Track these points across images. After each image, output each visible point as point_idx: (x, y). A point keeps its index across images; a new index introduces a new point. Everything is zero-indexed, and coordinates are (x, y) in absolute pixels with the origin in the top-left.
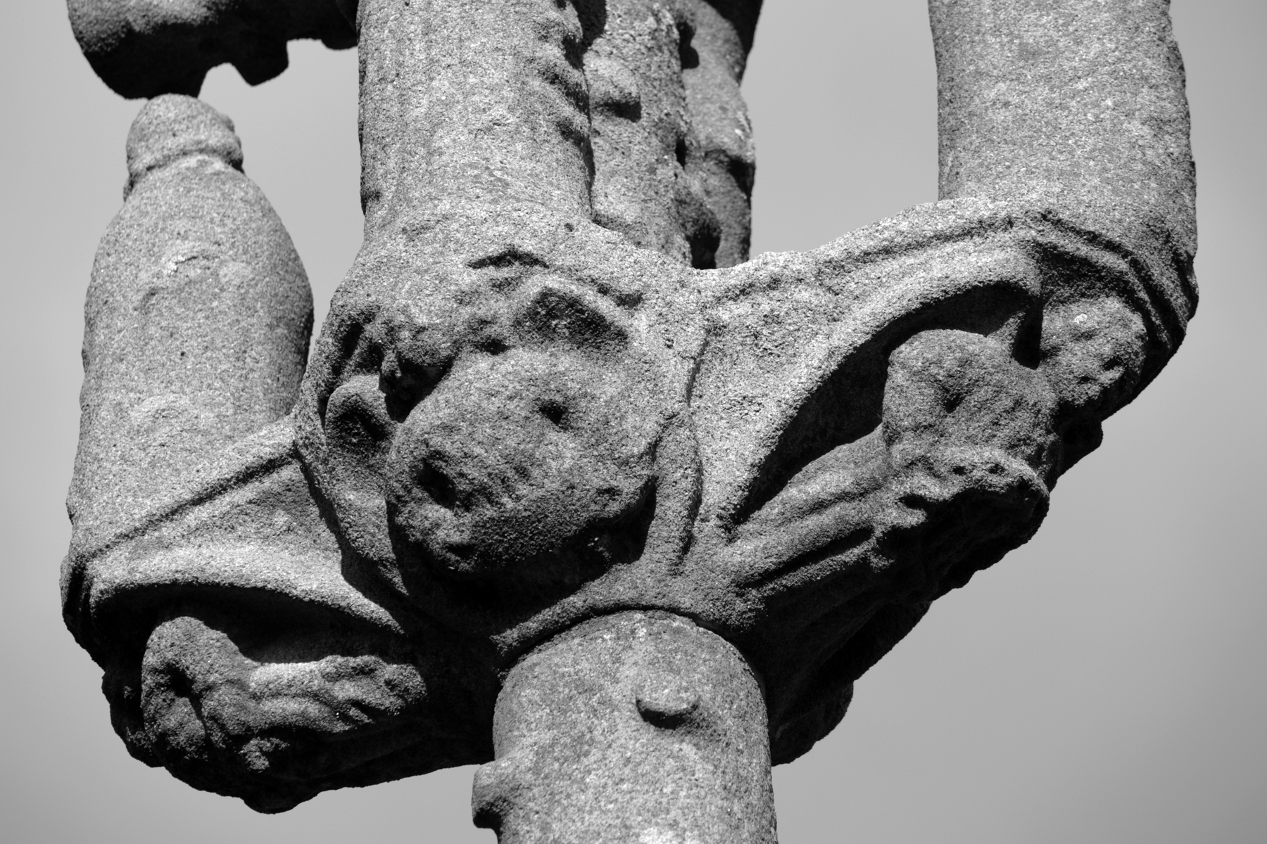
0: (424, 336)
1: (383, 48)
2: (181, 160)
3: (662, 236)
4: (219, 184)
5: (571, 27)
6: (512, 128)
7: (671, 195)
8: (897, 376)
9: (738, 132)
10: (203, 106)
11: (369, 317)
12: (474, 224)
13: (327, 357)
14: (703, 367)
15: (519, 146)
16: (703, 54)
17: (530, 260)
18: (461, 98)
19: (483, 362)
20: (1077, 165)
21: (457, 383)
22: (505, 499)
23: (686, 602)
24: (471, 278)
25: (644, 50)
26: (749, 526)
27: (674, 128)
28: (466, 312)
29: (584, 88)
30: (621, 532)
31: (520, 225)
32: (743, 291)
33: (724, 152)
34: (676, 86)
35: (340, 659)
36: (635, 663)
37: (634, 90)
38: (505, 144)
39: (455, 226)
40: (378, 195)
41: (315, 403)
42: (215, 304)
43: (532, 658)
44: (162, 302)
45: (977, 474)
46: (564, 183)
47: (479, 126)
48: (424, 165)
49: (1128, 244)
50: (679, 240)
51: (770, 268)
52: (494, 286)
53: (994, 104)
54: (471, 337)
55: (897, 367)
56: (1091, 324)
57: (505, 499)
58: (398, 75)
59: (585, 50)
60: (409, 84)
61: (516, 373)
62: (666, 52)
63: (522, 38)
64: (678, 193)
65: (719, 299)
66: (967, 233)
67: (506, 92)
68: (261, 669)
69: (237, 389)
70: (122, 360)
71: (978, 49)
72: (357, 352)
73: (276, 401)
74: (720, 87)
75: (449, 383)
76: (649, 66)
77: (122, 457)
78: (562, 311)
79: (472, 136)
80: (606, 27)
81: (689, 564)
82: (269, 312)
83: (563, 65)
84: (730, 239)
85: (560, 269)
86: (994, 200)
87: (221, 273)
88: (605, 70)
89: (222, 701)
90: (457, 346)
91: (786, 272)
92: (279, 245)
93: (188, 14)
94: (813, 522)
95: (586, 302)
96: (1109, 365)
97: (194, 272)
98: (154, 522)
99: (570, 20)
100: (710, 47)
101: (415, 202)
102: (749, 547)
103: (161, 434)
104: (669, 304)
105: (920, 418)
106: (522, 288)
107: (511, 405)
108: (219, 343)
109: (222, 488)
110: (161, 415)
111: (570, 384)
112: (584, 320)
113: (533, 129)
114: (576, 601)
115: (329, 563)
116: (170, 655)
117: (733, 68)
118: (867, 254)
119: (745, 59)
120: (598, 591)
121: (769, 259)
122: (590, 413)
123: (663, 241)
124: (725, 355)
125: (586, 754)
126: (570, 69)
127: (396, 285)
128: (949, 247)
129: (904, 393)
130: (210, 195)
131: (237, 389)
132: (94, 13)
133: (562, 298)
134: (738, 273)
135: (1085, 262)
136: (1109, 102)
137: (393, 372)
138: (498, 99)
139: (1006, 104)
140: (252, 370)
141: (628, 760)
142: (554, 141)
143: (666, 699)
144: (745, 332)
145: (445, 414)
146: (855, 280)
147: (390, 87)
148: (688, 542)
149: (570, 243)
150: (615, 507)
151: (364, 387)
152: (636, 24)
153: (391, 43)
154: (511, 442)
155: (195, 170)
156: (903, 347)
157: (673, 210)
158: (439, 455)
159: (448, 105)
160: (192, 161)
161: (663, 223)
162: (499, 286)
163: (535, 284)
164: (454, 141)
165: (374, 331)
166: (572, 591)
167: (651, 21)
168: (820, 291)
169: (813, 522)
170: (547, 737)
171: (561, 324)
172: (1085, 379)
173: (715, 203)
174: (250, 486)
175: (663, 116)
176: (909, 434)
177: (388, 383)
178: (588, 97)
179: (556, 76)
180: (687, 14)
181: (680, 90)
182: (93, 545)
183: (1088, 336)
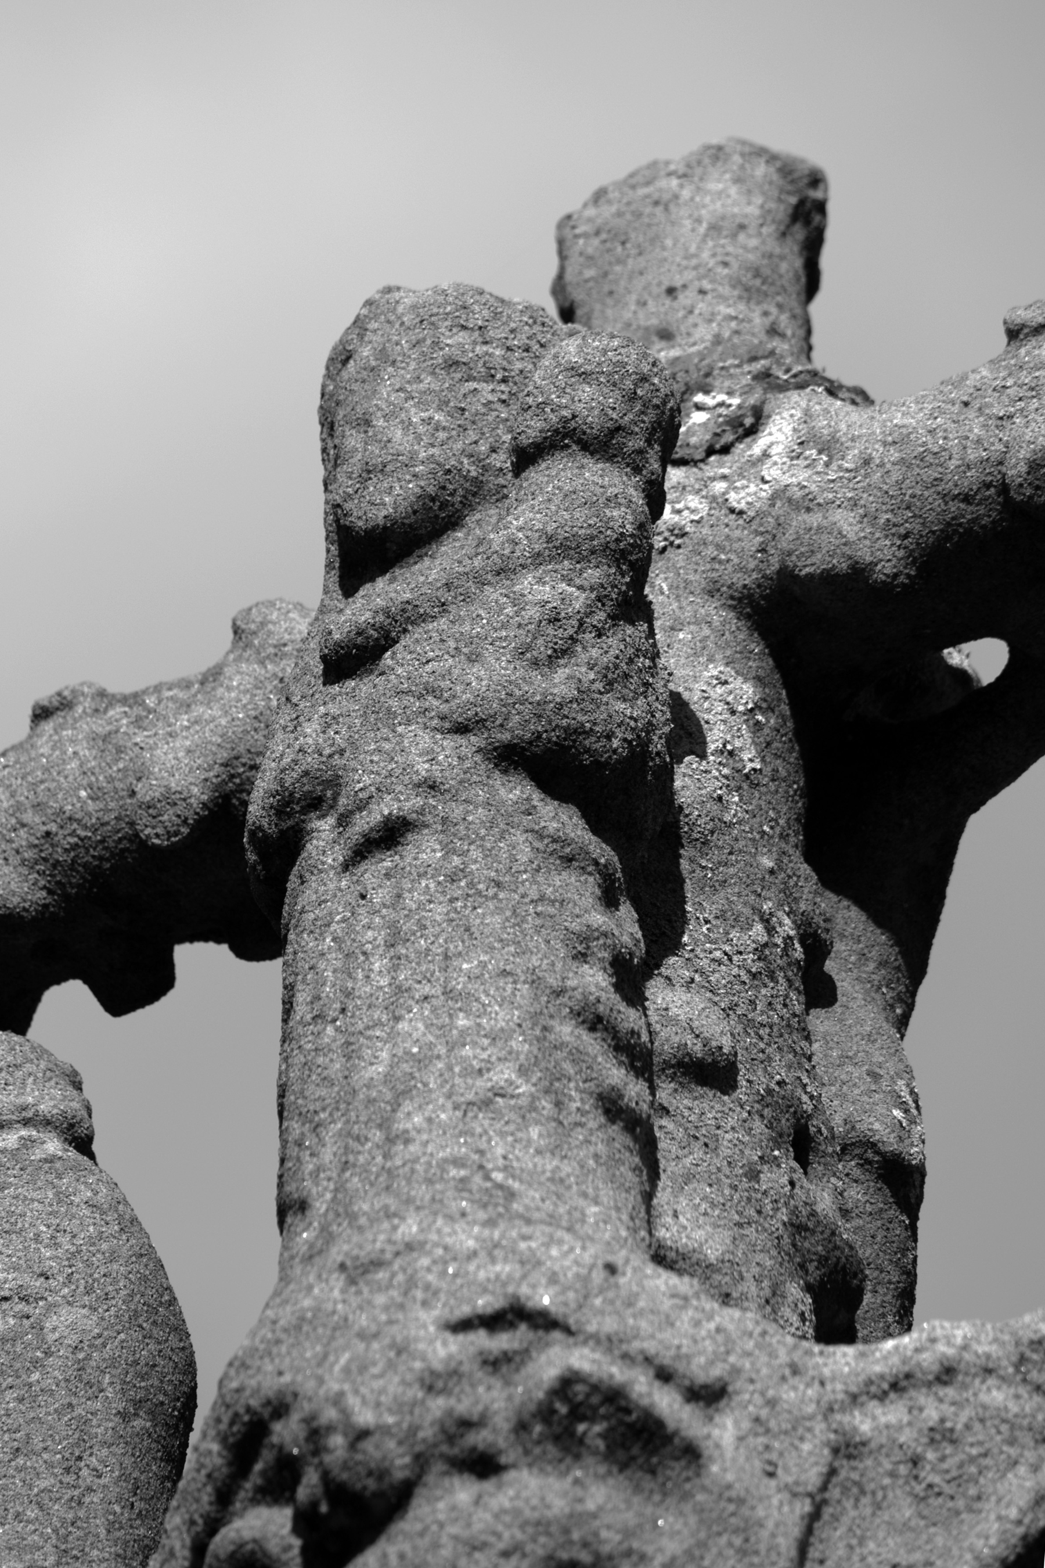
1: (322, 965)
3: (766, 1283)
4: (51, 1177)
5: (626, 939)
6: (523, 1102)
7: (783, 1215)
9: (897, 1113)
10: (33, 1049)
11: (279, 1408)
12: (455, 1259)
13: (209, 1476)
14: (827, 1512)
15: (534, 1132)
16: (844, 984)
17: (544, 1322)
18: (442, 1050)
19: (463, 1491)
21: (418, 1527)
24: (446, 1349)
25: (745, 977)
27: (791, 1105)
28: (438, 1405)
29: (645, 1037)
31: (530, 1263)
32: (895, 1386)
33: (874, 1145)
34: (795, 1036)
37: (726, 1042)
38: (512, 1127)
40: (303, 1206)
41: (187, 1553)
42: (35, 1376)
46: (607, 1194)
47: (470, 1096)
48: (379, 1159)
50: (794, 1290)
51: (941, 1348)
52: (485, 1362)
54: (444, 1448)
58: (343, 1010)
59: (649, 976)
60: (360, 1026)
61: (516, 1512)
62: (781, 980)
63: (546, 956)
64: (794, 1212)
67: (518, 1043)
69: (63, 1521)
72: (258, 1467)
73: (126, 1543)
74: (870, 1038)
75: (408, 1525)
76: (752, 1002)
78: (595, 1409)
79: (459, 1114)
80: (685, 939)
82: (123, 1391)
83: (610, 999)
84: (881, 1290)
85: (595, 1339)
88: (680, 1008)
90: (421, 1462)
91: (967, 1356)
92: (145, 1279)
93: (16, 900)
95: (634, 1396)
99: (625, 926)
100: (855, 973)
101: (363, 1221)
106: (530, 1368)
108: (37, 1443)
111: (604, 1534)
112: (630, 1426)
113: (558, 1104)
117: (892, 1007)
119: (913, 994)
121: (939, 1332)
123: (767, 1292)
124: (863, 1492)
126: (622, 1007)
127: (325, 1356)
130: (35, 1195)
131: (63, 1521)
133: (595, 1388)
134: (889, 1352)
137: (314, 1505)
140: (90, 1489)
142: (592, 1124)
144: (898, 1455)
149: (611, 1294)
152: (734, 934)
153: (335, 959)
155: (14, 1153)
157: (786, 1240)
159: (422, 1061)
161: (769, 1263)
162: (496, 1364)
163: (553, 1361)
164: (430, 1120)
165: (286, 1433)
167: (758, 929)
168: (1023, 1391)
171: (593, 1431)
173: (857, 1230)
175: (773, 1085)
177: (305, 1522)
178: (650, 1053)
179: (599, 1019)
180: (818, 920)
181: (803, 1043)
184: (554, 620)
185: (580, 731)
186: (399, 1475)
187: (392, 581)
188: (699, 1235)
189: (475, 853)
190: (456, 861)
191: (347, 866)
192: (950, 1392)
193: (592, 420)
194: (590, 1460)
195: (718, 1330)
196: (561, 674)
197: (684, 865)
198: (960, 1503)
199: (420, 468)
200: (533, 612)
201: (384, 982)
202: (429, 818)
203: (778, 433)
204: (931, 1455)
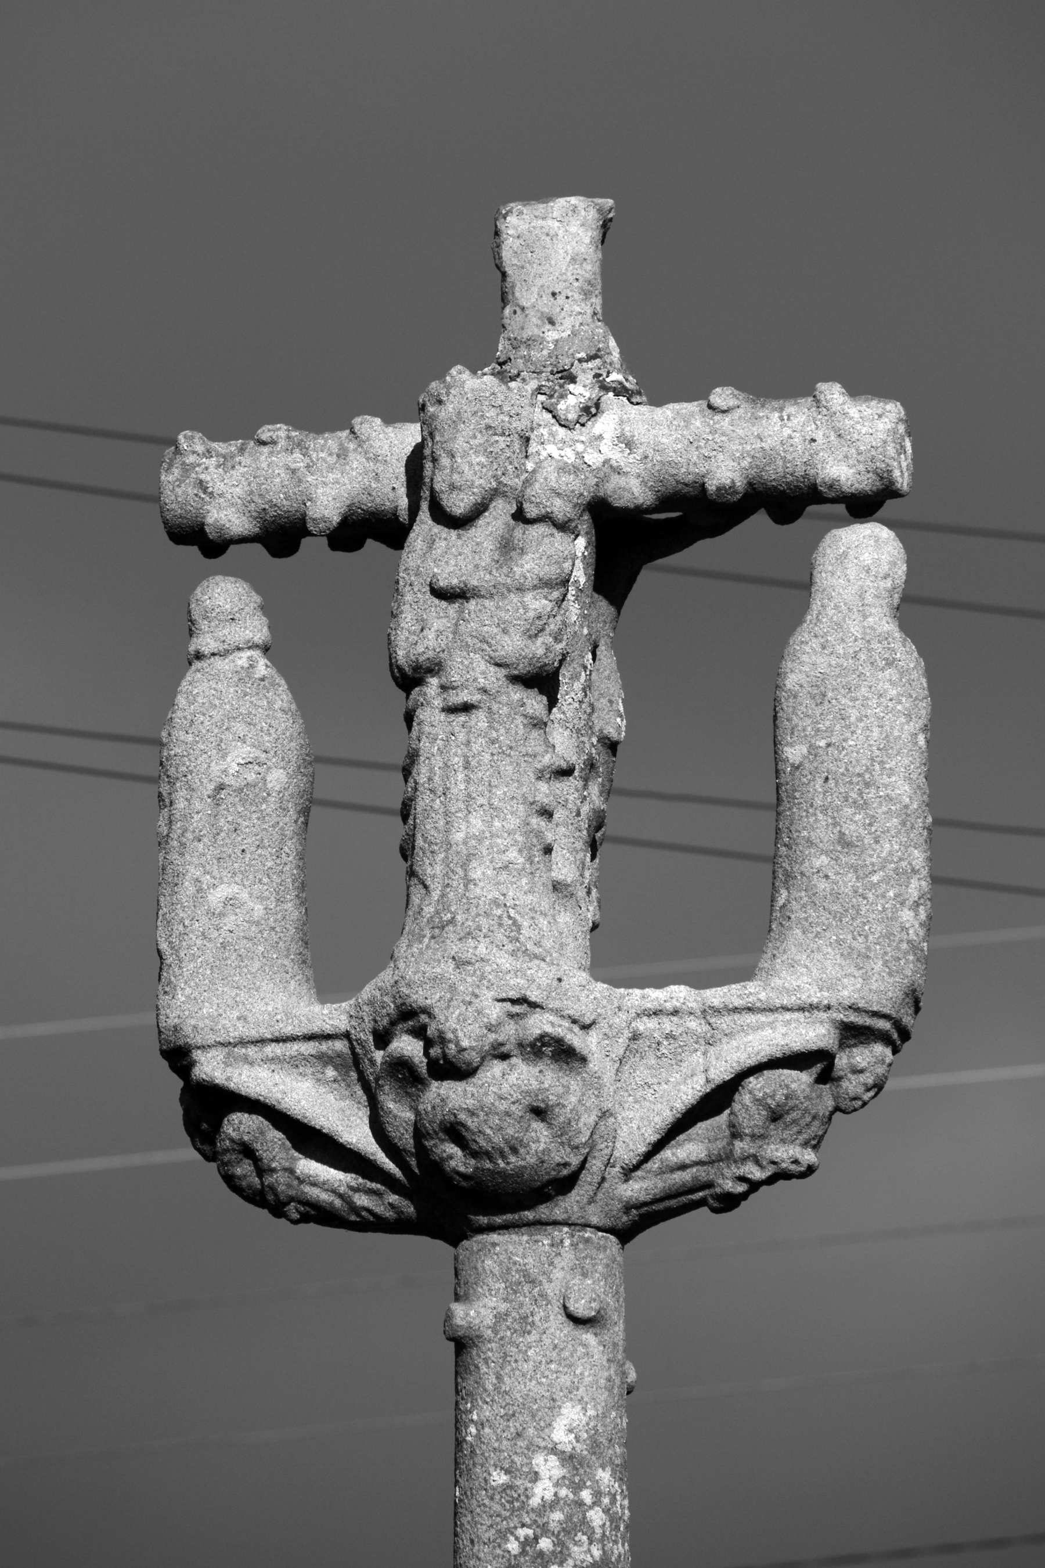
15: (524, 881)
17: (534, 1005)
19: (497, 1068)
20: (868, 948)
22: (500, 1161)
23: (594, 1220)
26: (639, 1173)
30: (565, 1183)
32: (655, 1013)
35: (361, 1180)
36: (563, 1268)
42: (264, 806)
43: (494, 1237)
45: (784, 1165)
53: (818, 872)
56: (864, 1064)
65: (638, 1015)
66: (801, 1009)
70: (200, 840)
81: (600, 1195)
85: (552, 1010)
86: (821, 990)
87: (269, 779)
89: (279, 1180)
96: (868, 1090)
97: (251, 777)
98: (243, 1043)
102: (637, 1186)
103: (229, 922)
105: (756, 1131)
107: (513, 1108)
109: (293, 1039)
110: (230, 902)
111: (551, 1097)
114: (529, 1215)
115: (360, 1114)
116: (246, 1138)
120: (543, 1211)
122: (561, 1116)
125: (529, 1333)
128: (788, 1016)
132: (179, 511)
133: (552, 1038)
136: (891, 894)
138: (512, 842)
139: (827, 877)
143: (581, 1308)
145: (470, 1102)
146: (724, 1022)
147: (438, 801)
150: (565, 1172)
151: (407, 1046)
154: (510, 1131)
156: (751, 1079)
158: (464, 1125)
160: (242, 659)
162: (512, 1016)
163: (539, 1024)
166: (528, 1208)
170: (503, 1307)
171: (548, 1050)
172: (855, 1099)
176: (748, 1139)
182: (198, 1040)
183: (861, 1071)
185: (546, 665)
186: (475, 1065)
188: (564, 871)
190: (494, 734)
191: (443, 710)
192: (675, 1019)
193: (560, 517)
195: (595, 999)
196: (540, 640)
199: (475, 490)
200: (531, 614)
201: (462, 787)
202: (482, 705)
203: (605, 425)
204: (665, 1043)
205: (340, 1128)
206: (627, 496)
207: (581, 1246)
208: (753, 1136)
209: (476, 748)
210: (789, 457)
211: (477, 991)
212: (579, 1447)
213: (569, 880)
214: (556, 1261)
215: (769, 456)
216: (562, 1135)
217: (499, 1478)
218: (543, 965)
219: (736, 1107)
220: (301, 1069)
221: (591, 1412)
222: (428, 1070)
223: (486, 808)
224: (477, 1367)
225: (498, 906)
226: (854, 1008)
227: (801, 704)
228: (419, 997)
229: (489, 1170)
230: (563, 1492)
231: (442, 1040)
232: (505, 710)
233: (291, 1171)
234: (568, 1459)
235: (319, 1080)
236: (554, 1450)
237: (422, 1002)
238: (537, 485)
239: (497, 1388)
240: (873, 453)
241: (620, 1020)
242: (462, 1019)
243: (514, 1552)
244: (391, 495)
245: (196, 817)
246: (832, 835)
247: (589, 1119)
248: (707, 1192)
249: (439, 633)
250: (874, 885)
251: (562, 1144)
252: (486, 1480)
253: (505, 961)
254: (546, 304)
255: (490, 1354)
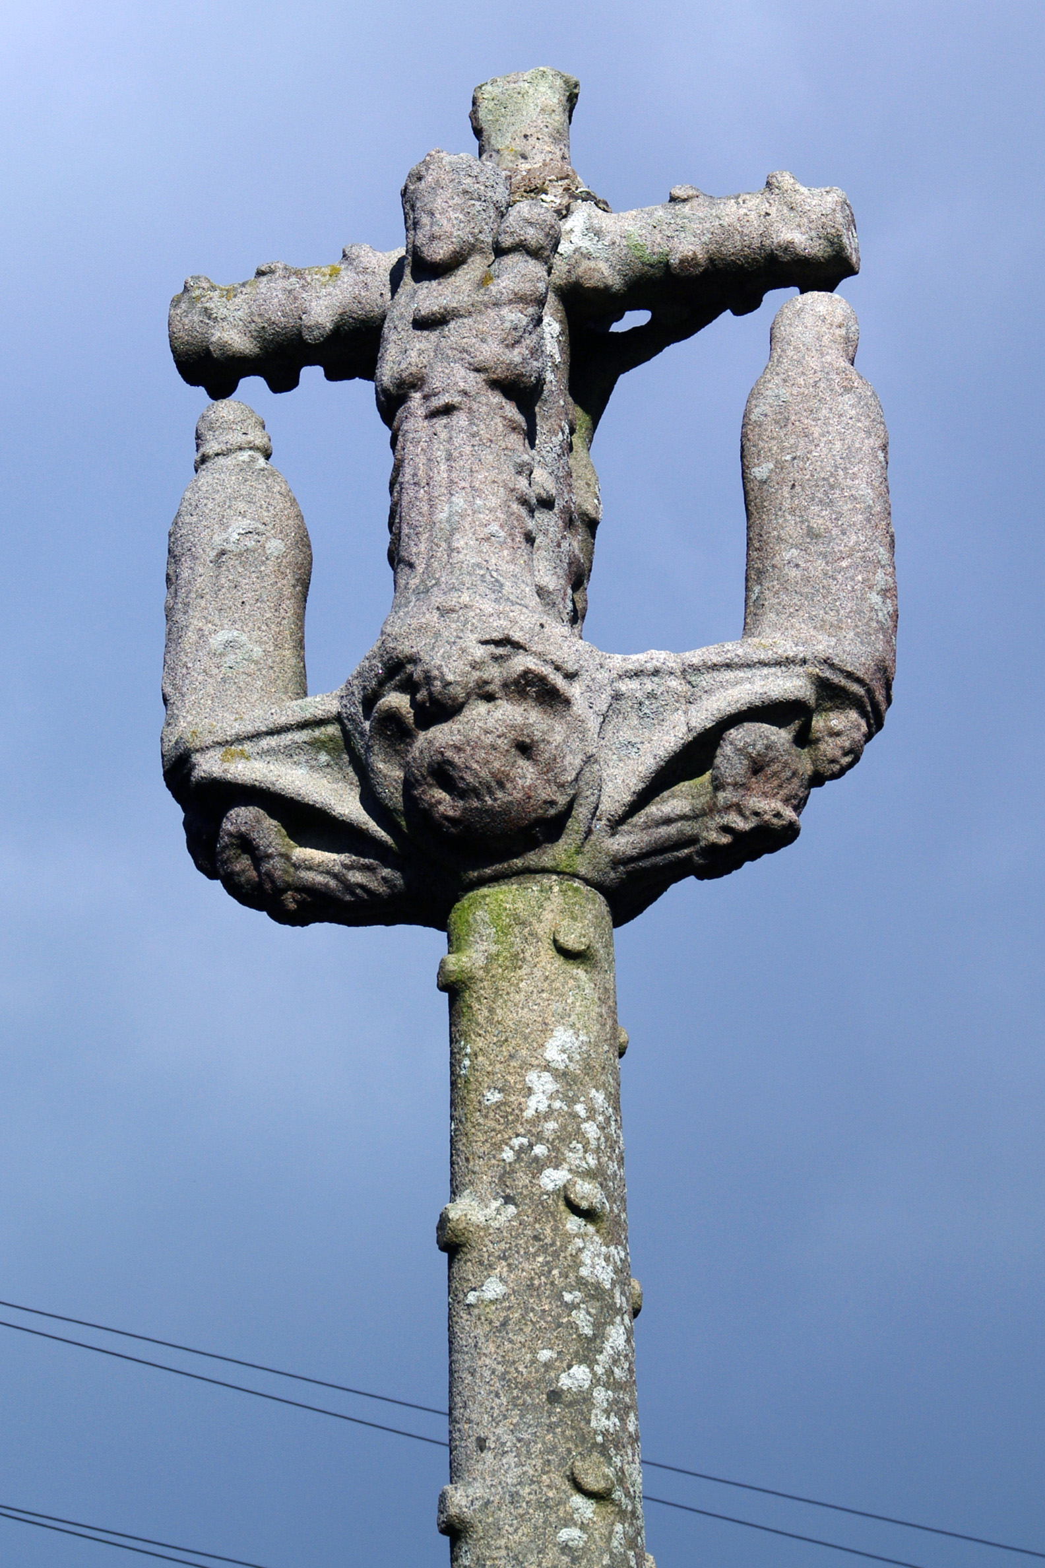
0: (451, 688)
2: (238, 453)
6: (502, 539)
8: (727, 749)
15: (506, 552)
17: (517, 646)
18: (469, 512)
19: (482, 707)
20: (840, 621)
22: (487, 798)
23: (583, 871)
26: (625, 827)
30: (552, 826)
31: (514, 622)
32: (636, 674)
35: (354, 857)
39: (472, 614)
42: (263, 568)
43: (484, 890)
44: (230, 561)
45: (766, 817)
49: (867, 679)
55: (727, 743)
56: (840, 727)
57: (487, 798)
66: (778, 664)
68: (299, 849)
71: (780, 521)
77: (204, 671)
81: (587, 848)
85: (535, 653)
86: (797, 645)
94: (664, 831)
96: (845, 754)
97: (250, 543)
98: (239, 739)
103: (230, 659)
104: (593, 680)
105: (738, 779)
107: (499, 741)
110: (230, 644)
114: (518, 862)
115: (353, 793)
116: (243, 829)
118: (715, 665)
120: (532, 859)
125: (520, 968)
128: (765, 671)
129: (729, 758)
133: (536, 675)
135: (843, 689)
136: (860, 578)
137: (424, 703)
139: (797, 566)
141: (547, 977)
143: (571, 941)
145: (457, 739)
146: (706, 680)
148: (589, 832)
150: (552, 812)
151: (397, 700)
154: (497, 764)
156: (732, 731)
158: (450, 763)
160: (245, 456)
162: (496, 658)
163: (521, 663)
169: (664, 831)
170: (494, 949)
171: (532, 690)
174: (305, 732)
176: (731, 788)
179: (526, 501)
182: (198, 744)
183: (838, 734)
184: (515, 329)
185: (522, 375)
187: (439, 284)
188: (547, 579)
189: (482, 426)
190: (475, 429)
191: (426, 417)
192: (656, 679)
193: (533, 243)
194: (530, 700)
196: (516, 351)
197: (537, 409)
198: (656, 722)
200: (508, 325)
201: (445, 475)
205: (333, 802)
206: (597, 275)
207: (570, 893)
208: (736, 785)
209: (457, 441)
210: (746, 231)
211: (461, 635)
212: (572, 1066)
213: (551, 588)
214: (546, 904)
215: (727, 231)
216: (548, 772)
217: (494, 1097)
218: (524, 610)
219: (718, 761)
220: (296, 758)
221: (583, 1038)
222: (415, 719)
223: (469, 490)
224: (470, 1007)
225: (481, 568)
226: (827, 662)
227: (766, 430)
228: (405, 648)
229: (476, 808)
230: (557, 1104)
231: (428, 679)
232: (484, 409)
233: (287, 857)
234: (561, 1076)
235: (312, 767)
236: (547, 1068)
237: (408, 651)
238: (511, 218)
239: (489, 1020)
240: (824, 219)
241: (602, 676)
242: (447, 657)
243: (508, 1161)
244: (380, 301)
245: (199, 580)
246: (801, 530)
247: (573, 761)
248: (692, 849)
249: (421, 352)
250: (842, 569)
251: (548, 781)
252: (480, 1102)
253: (488, 607)
254: (519, 145)
255: (482, 992)
